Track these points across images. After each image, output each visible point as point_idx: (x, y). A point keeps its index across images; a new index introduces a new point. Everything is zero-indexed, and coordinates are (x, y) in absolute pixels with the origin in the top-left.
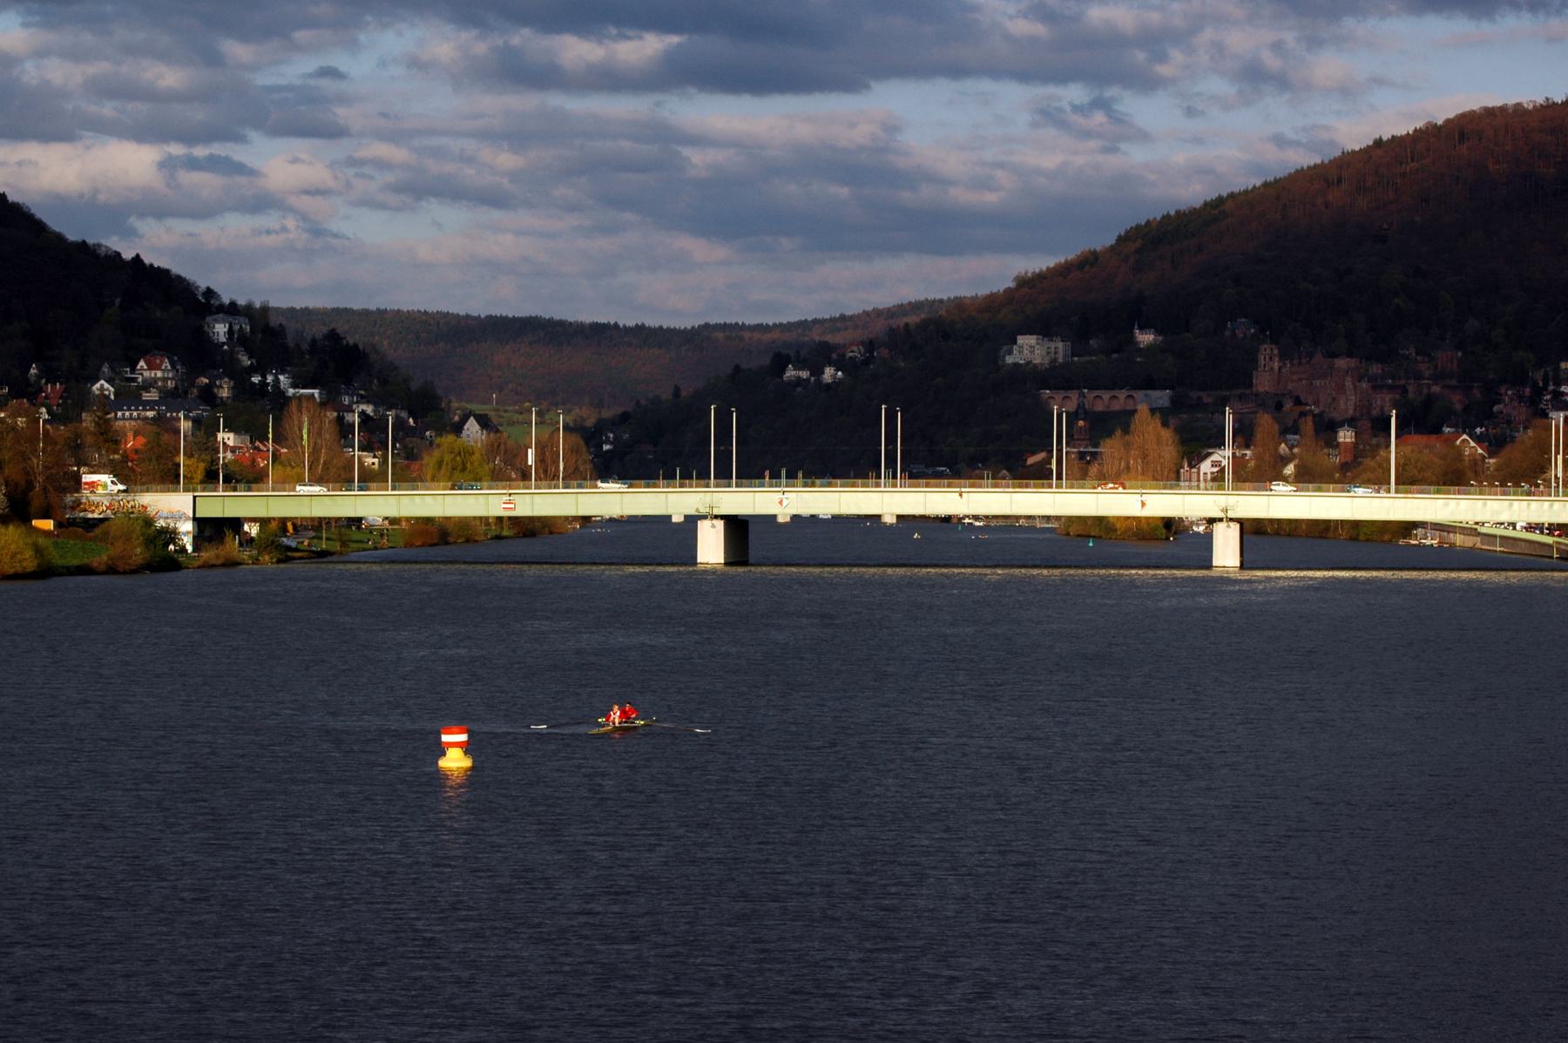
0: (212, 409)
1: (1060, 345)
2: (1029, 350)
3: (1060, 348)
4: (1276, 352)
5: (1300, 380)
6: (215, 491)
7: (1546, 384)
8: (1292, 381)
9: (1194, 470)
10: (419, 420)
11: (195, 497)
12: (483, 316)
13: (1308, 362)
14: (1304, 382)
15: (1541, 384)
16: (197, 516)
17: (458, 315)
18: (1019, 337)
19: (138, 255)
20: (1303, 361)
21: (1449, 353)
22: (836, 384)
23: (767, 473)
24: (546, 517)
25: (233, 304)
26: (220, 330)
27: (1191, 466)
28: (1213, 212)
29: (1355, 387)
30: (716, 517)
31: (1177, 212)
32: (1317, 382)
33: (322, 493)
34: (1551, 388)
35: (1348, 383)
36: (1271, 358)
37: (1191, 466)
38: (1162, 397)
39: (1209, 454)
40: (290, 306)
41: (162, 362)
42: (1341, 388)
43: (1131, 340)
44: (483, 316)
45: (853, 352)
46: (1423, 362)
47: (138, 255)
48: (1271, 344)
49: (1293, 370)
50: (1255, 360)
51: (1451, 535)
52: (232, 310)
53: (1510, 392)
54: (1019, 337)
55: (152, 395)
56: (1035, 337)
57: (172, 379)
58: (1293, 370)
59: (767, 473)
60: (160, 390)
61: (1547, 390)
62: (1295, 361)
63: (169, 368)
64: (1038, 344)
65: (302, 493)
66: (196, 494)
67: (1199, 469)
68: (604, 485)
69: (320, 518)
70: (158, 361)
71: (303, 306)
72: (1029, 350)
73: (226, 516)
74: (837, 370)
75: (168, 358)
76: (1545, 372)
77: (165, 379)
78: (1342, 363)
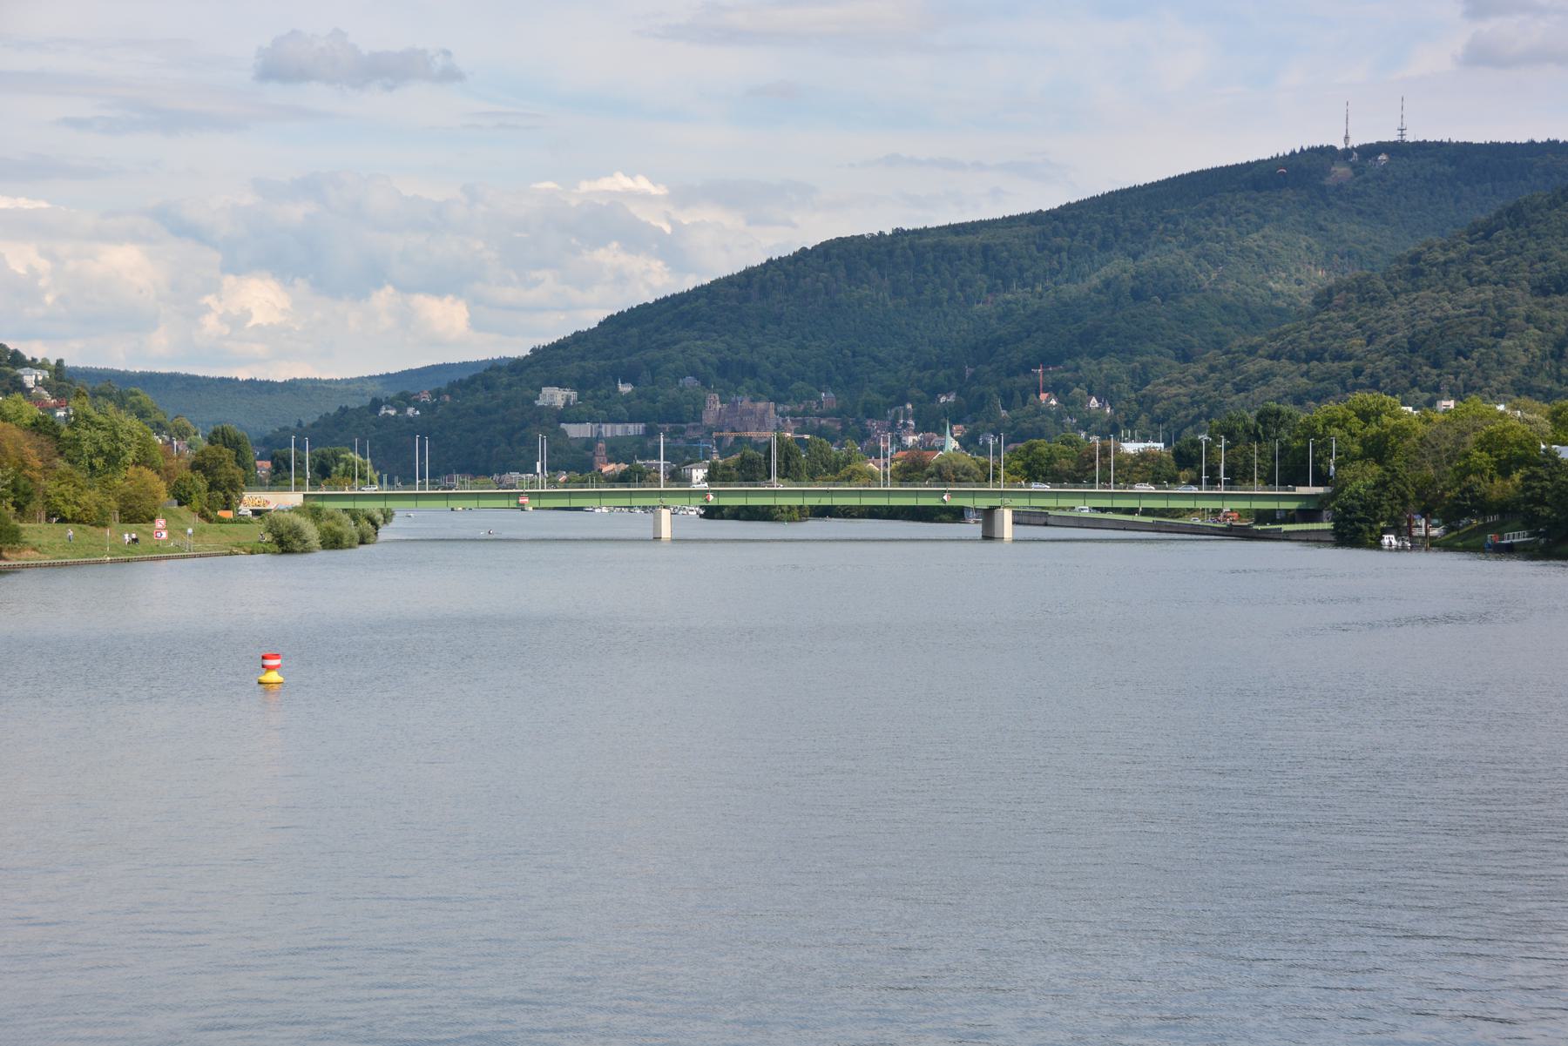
2: (556, 397)
25: (34, 360)
72: (556, 397)
74: (416, 410)
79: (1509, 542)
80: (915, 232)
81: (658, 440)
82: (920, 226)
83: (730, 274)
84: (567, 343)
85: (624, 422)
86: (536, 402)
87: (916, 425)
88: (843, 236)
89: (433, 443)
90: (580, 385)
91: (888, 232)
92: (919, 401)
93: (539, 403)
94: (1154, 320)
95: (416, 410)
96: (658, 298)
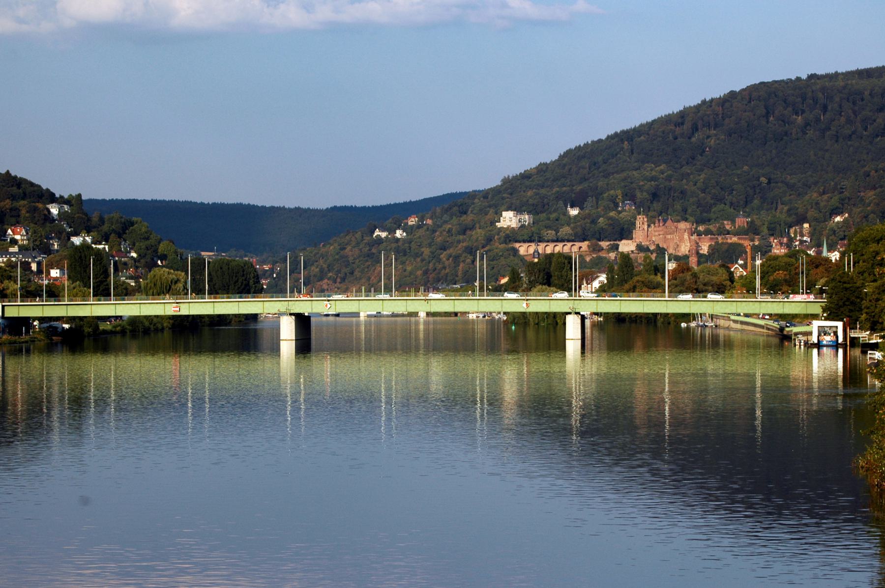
0: (48, 256)
1: (527, 217)
2: (509, 219)
3: (526, 218)
4: (646, 219)
5: (659, 235)
6: (16, 302)
7: (796, 236)
8: (655, 236)
9: (589, 286)
10: (164, 262)
11: (3, 307)
12: (210, 203)
13: (664, 225)
14: (661, 236)
15: (793, 236)
16: (6, 315)
17: (196, 203)
18: (503, 213)
19: (8, 171)
20: (661, 224)
21: (742, 219)
22: (403, 240)
23: (373, 289)
24: (223, 315)
25: (61, 197)
26: (54, 210)
27: (588, 284)
28: (612, 141)
29: (689, 238)
30: (291, 314)
31: (592, 142)
32: (669, 237)
33: (722, 299)
34: (798, 238)
35: (686, 236)
36: (643, 223)
37: (588, 284)
38: (235, 249)
39: (598, 277)
40: (103, 198)
41: (21, 231)
42: (681, 239)
43: (566, 213)
44: (210, 203)
45: (412, 221)
46: (728, 224)
47: (8, 171)
48: (643, 215)
49: (655, 229)
50: (634, 224)
51: (718, 320)
52: (61, 201)
53: (775, 241)
54: (503, 213)
55: (15, 249)
56: (512, 212)
57: (25, 240)
58: (655, 229)
59: (373, 289)
60: (20, 247)
61: (796, 239)
62: (656, 225)
63: (25, 234)
64: (514, 216)
65: (555, 298)
66: (4, 304)
67: (592, 285)
68: (509, 295)
69: (555, 313)
70: (18, 230)
71: (170, 199)
72: (509, 219)
73: (21, 315)
74: (403, 232)
75: (24, 228)
76: (795, 229)
77: (22, 240)
78: (683, 225)
79: (876, 341)
80: (827, 76)
81: (387, 262)
82: (832, 71)
83: (671, 112)
84: (531, 174)
85: (564, 241)
86: (497, 224)
87: (811, 241)
88: (776, 80)
89: (95, 268)
90: (533, 210)
91: (804, 77)
92: (816, 219)
93: (498, 225)
94: (545, 176)
95: (403, 232)
96: (610, 134)
